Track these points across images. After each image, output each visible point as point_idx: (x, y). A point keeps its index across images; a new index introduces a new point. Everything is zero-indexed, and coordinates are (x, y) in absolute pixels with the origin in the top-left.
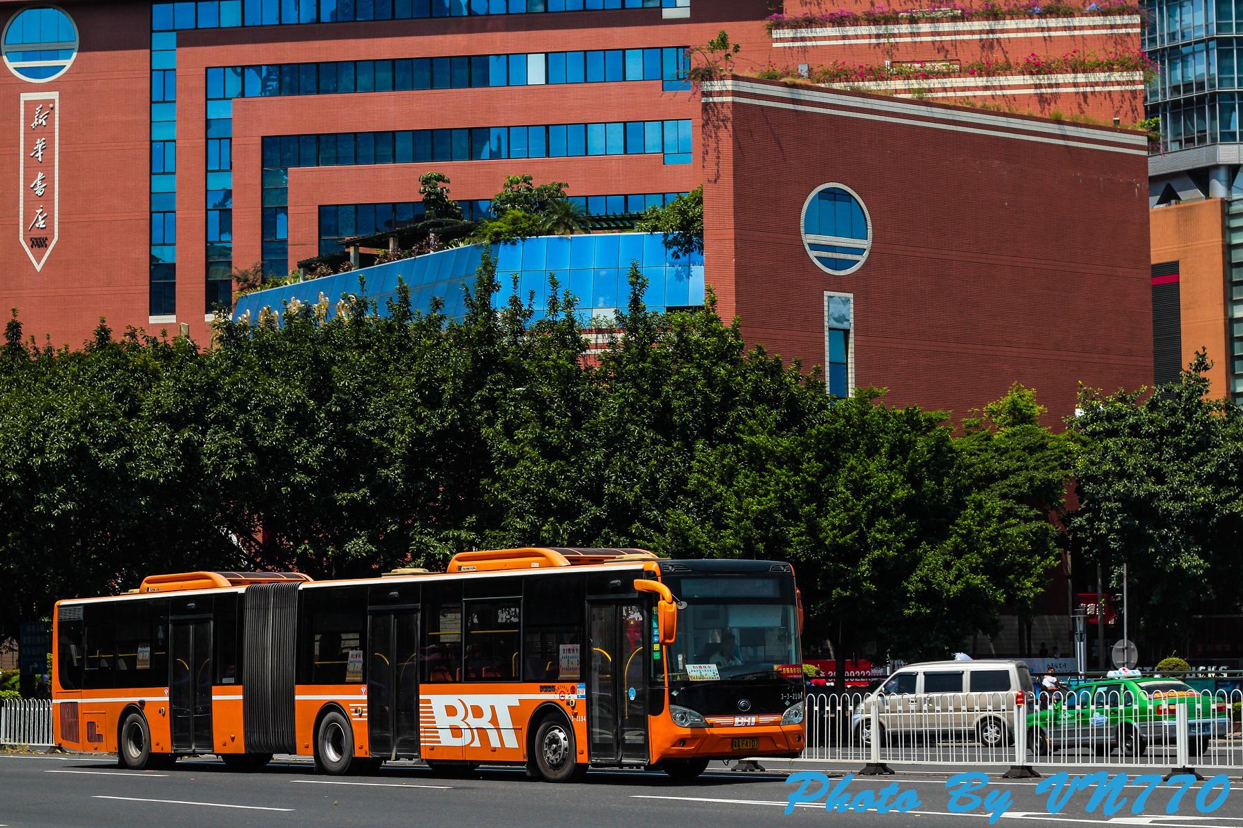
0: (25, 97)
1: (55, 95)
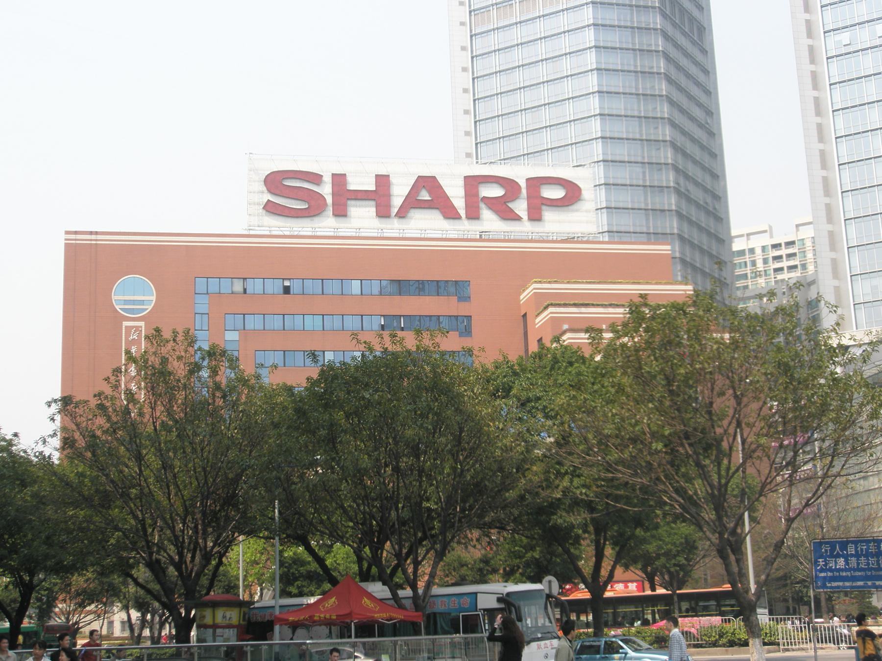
0: (126, 324)
1: (142, 324)
